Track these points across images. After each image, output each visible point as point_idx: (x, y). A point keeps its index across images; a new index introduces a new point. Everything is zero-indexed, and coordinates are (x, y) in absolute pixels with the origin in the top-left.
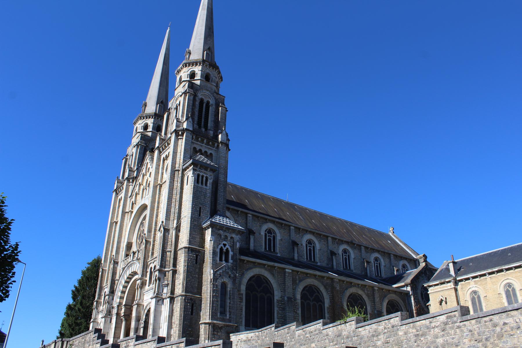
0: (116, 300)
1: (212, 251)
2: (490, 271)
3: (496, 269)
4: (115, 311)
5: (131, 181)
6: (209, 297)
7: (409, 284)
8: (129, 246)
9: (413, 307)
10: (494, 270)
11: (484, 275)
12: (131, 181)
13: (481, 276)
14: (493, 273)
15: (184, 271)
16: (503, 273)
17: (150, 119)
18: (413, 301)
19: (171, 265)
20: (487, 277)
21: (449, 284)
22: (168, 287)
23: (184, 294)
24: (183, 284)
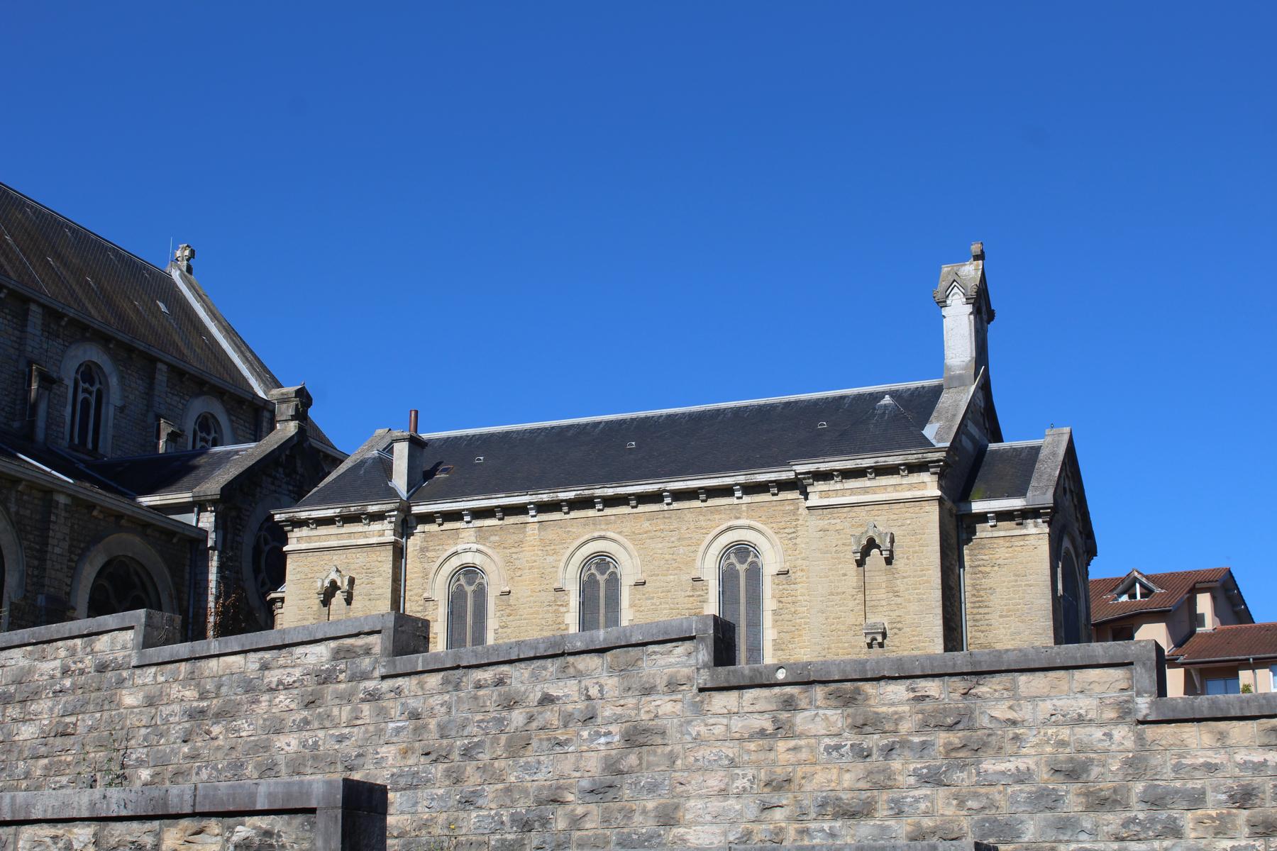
2: (545, 497)
3: (571, 495)
10: (598, 492)
11: (521, 510)
16: (591, 513)
21: (376, 526)
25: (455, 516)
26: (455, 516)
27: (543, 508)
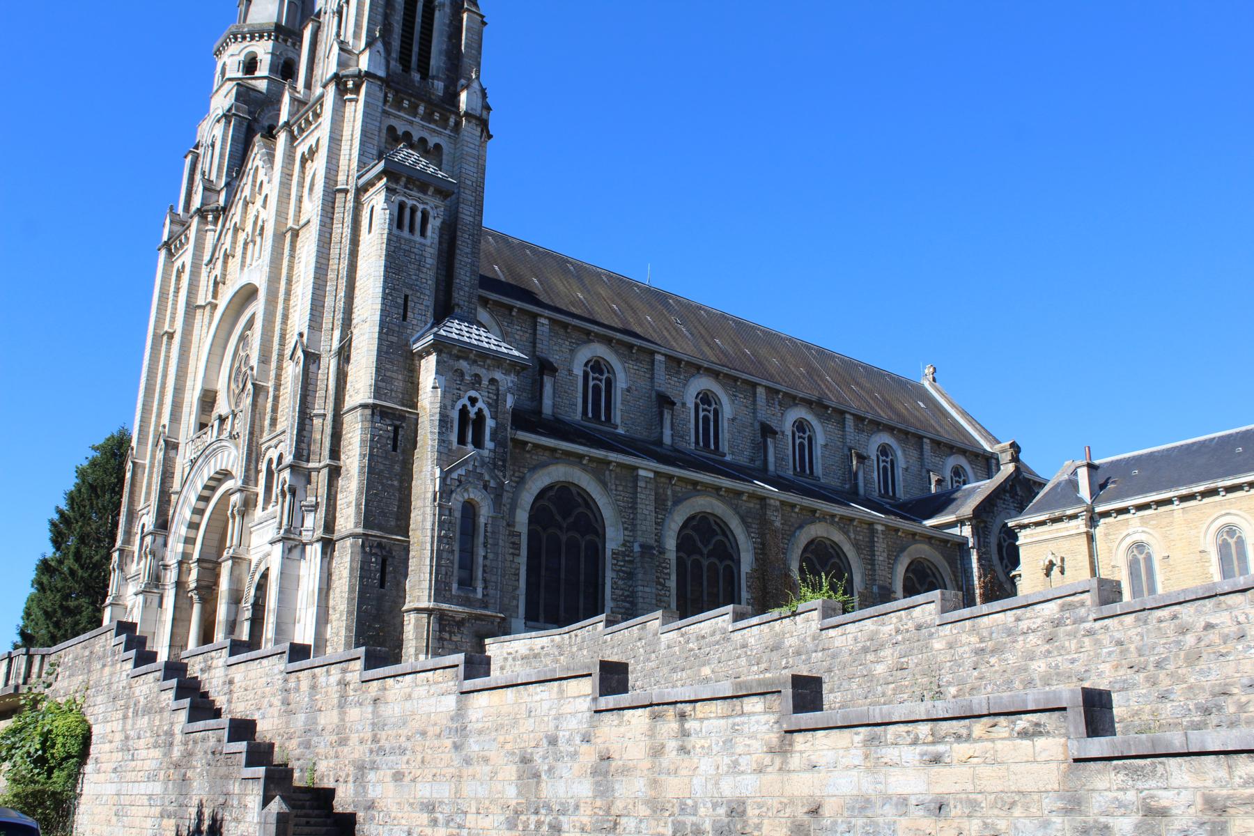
0: (175, 548)
1: (437, 417)
3: (1201, 488)
4: (171, 577)
5: (210, 218)
6: (429, 539)
7: (969, 519)
8: (208, 400)
9: (976, 579)
11: (1169, 502)
12: (210, 218)
13: (1160, 503)
14: (1191, 497)
15: (361, 468)
16: (1216, 498)
17: (263, 42)
18: (975, 565)
19: (326, 452)
20: (1177, 506)
21: (1074, 523)
22: (316, 511)
23: (360, 530)
24: (358, 505)
25: (1125, 511)
26: (1125, 511)
27: (1183, 499)
